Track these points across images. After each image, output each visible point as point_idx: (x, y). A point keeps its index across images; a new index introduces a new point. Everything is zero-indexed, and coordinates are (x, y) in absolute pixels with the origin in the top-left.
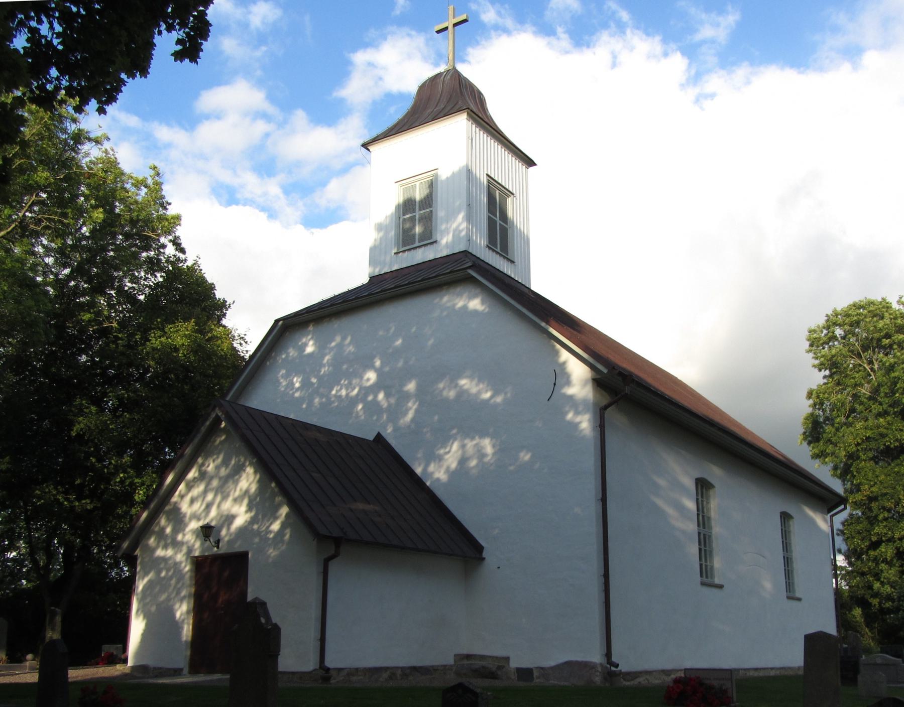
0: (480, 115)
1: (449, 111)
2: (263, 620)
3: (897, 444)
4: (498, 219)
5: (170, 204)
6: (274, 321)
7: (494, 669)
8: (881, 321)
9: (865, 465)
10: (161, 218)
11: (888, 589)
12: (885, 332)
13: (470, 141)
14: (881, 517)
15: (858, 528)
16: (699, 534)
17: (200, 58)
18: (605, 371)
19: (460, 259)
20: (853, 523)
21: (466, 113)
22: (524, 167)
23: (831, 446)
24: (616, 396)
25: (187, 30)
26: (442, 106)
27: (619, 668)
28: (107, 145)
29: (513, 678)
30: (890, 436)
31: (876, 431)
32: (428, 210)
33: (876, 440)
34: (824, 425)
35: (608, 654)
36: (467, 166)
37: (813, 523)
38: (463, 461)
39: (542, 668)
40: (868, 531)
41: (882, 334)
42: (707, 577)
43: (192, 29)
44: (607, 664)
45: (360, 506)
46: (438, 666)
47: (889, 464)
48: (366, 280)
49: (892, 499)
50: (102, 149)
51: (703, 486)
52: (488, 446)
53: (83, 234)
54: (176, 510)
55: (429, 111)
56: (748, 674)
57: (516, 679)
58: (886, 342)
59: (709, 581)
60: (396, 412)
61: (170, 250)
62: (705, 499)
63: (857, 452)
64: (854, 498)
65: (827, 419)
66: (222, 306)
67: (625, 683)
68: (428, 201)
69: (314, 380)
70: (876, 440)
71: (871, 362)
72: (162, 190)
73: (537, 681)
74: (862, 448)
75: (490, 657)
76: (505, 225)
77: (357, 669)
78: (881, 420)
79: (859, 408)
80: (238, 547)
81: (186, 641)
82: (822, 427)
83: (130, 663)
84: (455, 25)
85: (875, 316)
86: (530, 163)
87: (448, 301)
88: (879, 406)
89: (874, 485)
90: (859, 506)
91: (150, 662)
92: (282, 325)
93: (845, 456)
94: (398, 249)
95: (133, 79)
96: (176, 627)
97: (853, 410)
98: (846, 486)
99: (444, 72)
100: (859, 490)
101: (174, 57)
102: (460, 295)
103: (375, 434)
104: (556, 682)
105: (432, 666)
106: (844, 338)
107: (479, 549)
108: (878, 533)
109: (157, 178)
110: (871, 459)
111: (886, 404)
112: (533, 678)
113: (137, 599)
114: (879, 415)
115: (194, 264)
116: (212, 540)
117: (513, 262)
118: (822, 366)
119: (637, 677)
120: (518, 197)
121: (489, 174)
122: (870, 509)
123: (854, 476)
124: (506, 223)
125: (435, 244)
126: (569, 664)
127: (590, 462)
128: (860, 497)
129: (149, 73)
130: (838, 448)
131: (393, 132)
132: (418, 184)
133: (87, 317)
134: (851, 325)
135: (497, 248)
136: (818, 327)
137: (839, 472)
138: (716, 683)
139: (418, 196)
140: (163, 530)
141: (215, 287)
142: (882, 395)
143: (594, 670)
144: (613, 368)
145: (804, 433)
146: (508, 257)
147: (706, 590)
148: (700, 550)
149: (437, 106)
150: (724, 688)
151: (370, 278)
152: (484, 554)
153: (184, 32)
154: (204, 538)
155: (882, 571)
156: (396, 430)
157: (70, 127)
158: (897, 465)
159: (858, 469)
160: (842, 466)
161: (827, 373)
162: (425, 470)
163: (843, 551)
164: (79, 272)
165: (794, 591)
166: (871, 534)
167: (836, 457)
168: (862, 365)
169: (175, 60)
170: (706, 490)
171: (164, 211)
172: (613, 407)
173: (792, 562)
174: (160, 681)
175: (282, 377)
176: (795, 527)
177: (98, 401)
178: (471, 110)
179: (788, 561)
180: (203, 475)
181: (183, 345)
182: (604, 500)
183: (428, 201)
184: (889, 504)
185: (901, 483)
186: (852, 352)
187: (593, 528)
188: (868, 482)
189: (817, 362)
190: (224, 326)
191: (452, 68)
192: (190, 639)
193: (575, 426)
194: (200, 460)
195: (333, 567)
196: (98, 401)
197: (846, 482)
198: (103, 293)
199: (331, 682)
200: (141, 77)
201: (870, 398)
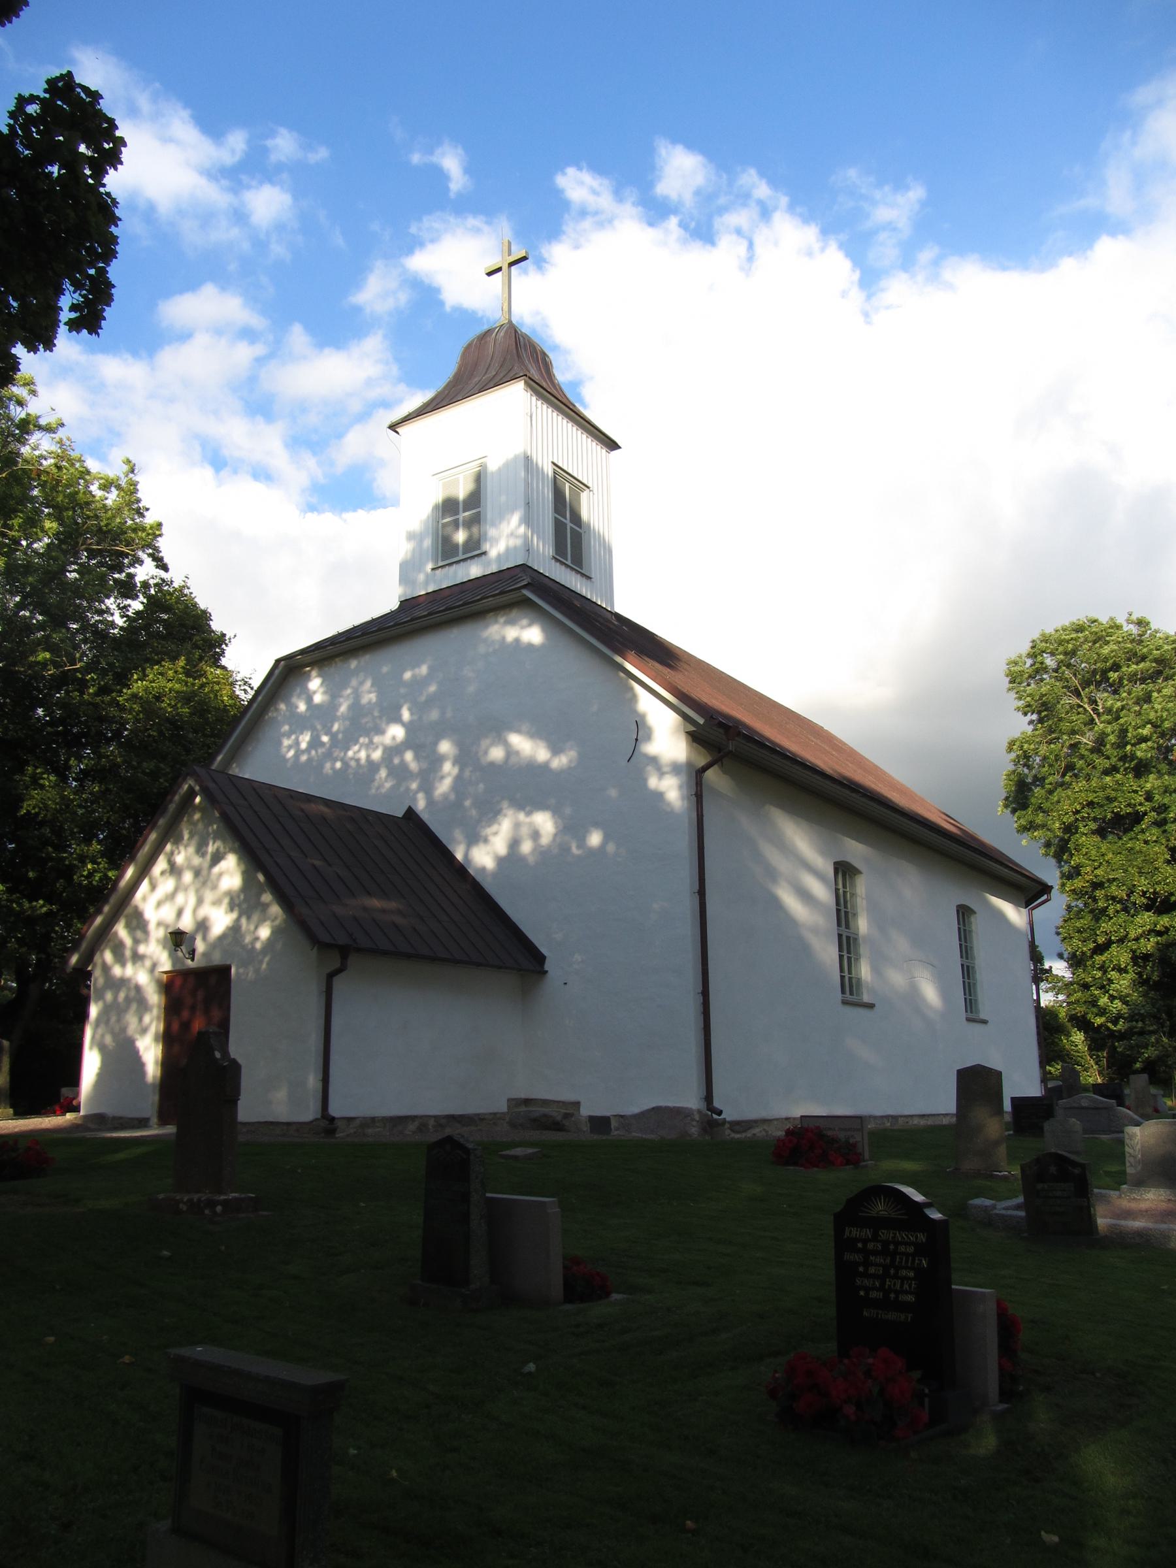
0: (544, 384)
1: (501, 379)
2: (218, 1055)
3: (1129, 810)
4: (568, 522)
5: (147, 509)
6: (274, 662)
7: (559, 1118)
8: (1106, 647)
9: (1086, 840)
10: (136, 529)
12: (1111, 661)
13: (529, 418)
14: (1111, 911)
15: (1078, 924)
16: (840, 936)
17: (102, 329)
18: (701, 721)
19: (515, 576)
20: (1072, 919)
22: (604, 451)
24: (719, 752)
25: (84, 292)
26: (494, 373)
28: (61, 434)
29: (585, 1129)
30: (1120, 799)
33: (1102, 806)
34: (1033, 788)
35: (709, 1098)
36: (525, 453)
37: (1000, 916)
38: (514, 844)
39: (622, 1116)
41: (1108, 664)
42: (851, 993)
43: (89, 292)
44: (708, 1110)
45: (376, 903)
46: (485, 1114)
47: (1120, 838)
48: (394, 605)
49: (1123, 885)
50: (55, 438)
51: (844, 871)
52: (545, 822)
55: (477, 379)
56: (910, 1123)
57: (589, 1130)
58: (1113, 676)
59: (854, 998)
62: (848, 889)
63: (1076, 822)
65: (1035, 778)
66: (221, 640)
67: (733, 1135)
69: (325, 739)
70: (1102, 806)
72: (138, 490)
73: (616, 1133)
75: (555, 1102)
76: (578, 529)
77: (373, 1119)
78: (1108, 779)
79: (1080, 763)
80: (217, 959)
81: (153, 1085)
84: (511, 264)
86: (612, 445)
88: (1105, 760)
89: (1099, 866)
90: (1080, 895)
92: (285, 666)
94: (437, 561)
95: (35, 353)
97: (1070, 767)
98: (1062, 869)
100: (1079, 874)
102: (512, 622)
103: (405, 809)
104: (640, 1135)
105: (478, 1115)
106: (1056, 671)
107: (540, 958)
108: (1106, 932)
109: (131, 475)
110: (1094, 832)
111: (1115, 757)
112: (611, 1129)
114: (1106, 772)
116: (184, 950)
117: (589, 578)
118: (1028, 709)
119: (750, 1128)
120: (595, 491)
121: (556, 462)
122: (1095, 900)
124: (580, 526)
125: (483, 556)
126: (657, 1110)
128: (1081, 884)
129: (55, 345)
130: (1050, 818)
131: (429, 409)
132: (461, 477)
135: (567, 560)
136: (1020, 657)
137: (1053, 849)
138: (842, 1136)
139: (462, 492)
141: (211, 616)
143: (689, 1118)
144: (712, 717)
145: (1007, 799)
146: (582, 572)
148: (841, 957)
149: (486, 372)
150: (851, 1141)
151: (401, 602)
152: (547, 967)
153: (80, 295)
154: (174, 947)
156: (430, 802)
157: (14, 411)
158: (1130, 839)
159: (1077, 845)
160: (1056, 842)
161: (1035, 717)
162: (466, 855)
165: (977, 1011)
167: (1048, 830)
168: (1082, 706)
170: (850, 877)
171: (141, 519)
172: (716, 767)
174: (115, 1135)
176: (978, 924)
177: (62, 773)
178: (529, 378)
179: (968, 972)
182: (702, 893)
183: (475, 499)
185: (1135, 863)
187: (687, 930)
189: (1021, 703)
190: (224, 668)
191: (507, 321)
193: (659, 796)
194: (168, 847)
195: (339, 983)
196: (62, 773)
197: (1063, 863)
199: (337, 1136)
200: (45, 351)
201: (1092, 751)
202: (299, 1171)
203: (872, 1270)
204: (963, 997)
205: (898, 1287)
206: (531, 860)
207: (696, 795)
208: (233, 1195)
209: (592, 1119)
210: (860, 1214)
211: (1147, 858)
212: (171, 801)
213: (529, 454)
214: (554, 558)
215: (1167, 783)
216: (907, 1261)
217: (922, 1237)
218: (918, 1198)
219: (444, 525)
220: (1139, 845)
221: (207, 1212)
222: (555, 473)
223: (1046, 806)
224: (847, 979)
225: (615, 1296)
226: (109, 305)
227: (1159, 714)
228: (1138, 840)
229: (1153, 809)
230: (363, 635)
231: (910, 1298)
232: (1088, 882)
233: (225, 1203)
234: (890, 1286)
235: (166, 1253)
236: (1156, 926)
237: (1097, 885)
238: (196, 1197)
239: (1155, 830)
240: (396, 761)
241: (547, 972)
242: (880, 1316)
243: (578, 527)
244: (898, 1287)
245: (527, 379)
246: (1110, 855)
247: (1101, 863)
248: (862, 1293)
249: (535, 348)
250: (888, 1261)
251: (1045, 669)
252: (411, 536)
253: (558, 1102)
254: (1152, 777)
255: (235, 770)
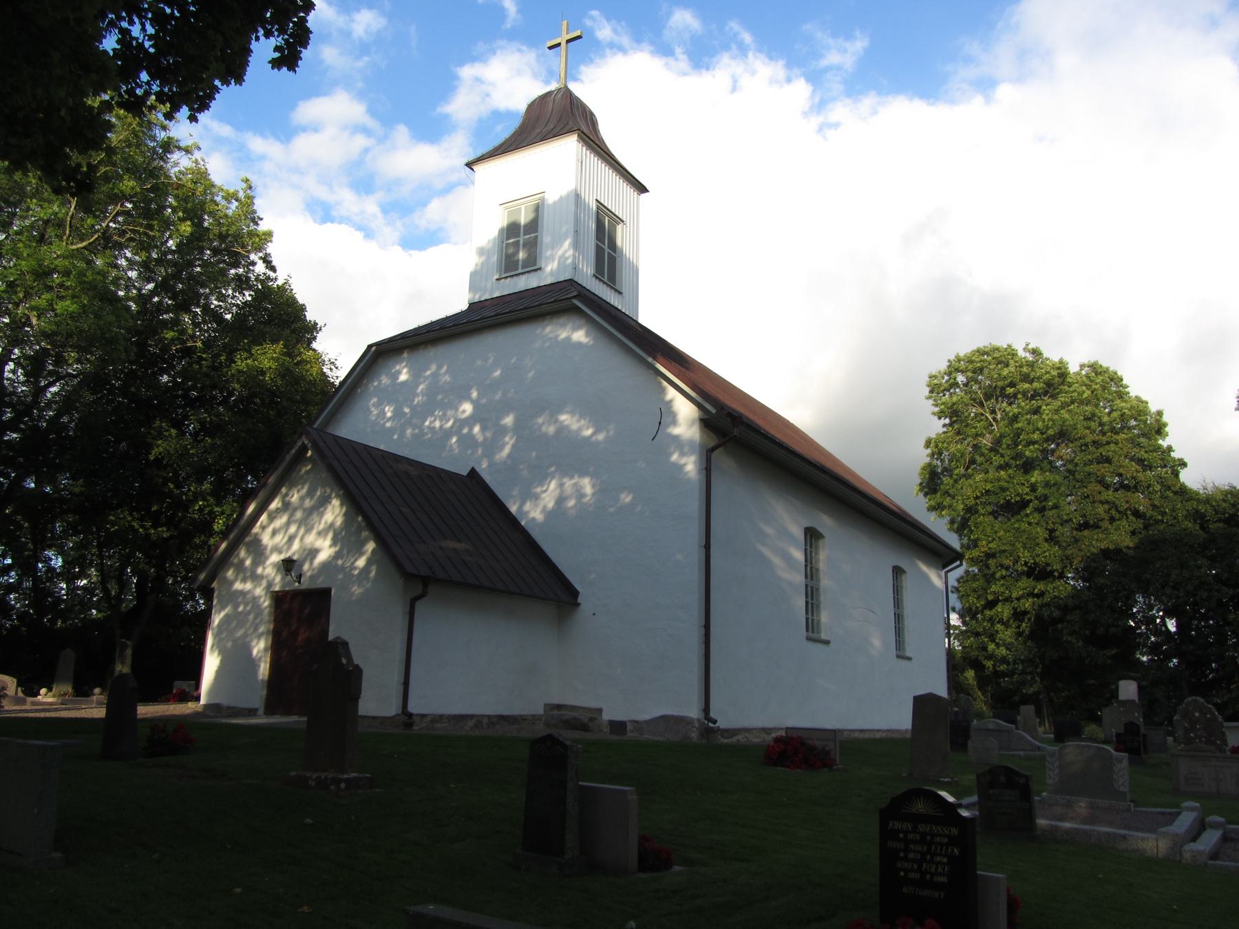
0: (591, 137)
2: (344, 661)
3: (1018, 499)
4: (606, 247)
5: (261, 219)
7: (586, 721)
10: (252, 234)
11: (1003, 651)
13: (580, 164)
14: (998, 575)
15: (974, 585)
16: (807, 586)
18: (714, 411)
21: (577, 135)
23: (948, 498)
24: (724, 437)
25: (286, 37)
26: (552, 126)
27: (717, 725)
28: (197, 155)
29: (605, 730)
31: (996, 484)
32: (533, 235)
33: (996, 494)
34: (942, 476)
35: (706, 710)
36: (576, 190)
38: (560, 500)
39: (636, 722)
40: (985, 590)
42: (813, 632)
45: (451, 544)
46: (527, 715)
49: (1011, 556)
51: (812, 535)
53: (169, 248)
54: (257, 541)
58: (1010, 390)
59: (815, 636)
60: (492, 446)
61: (260, 268)
64: (971, 554)
65: (945, 469)
67: (722, 740)
68: (533, 226)
69: (407, 410)
70: (996, 494)
71: (993, 412)
74: (981, 502)
75: (581, 708)
76: (613, 254)
77: (441, 716)
78: (1002, 473)
79: (979, 459)
80: (321, 583)
82: (940, 478)
83: (203, 701)
84: (568, 41)
85: (1000, 363)
86: (642, 189)
87: (550, 332)
89: (993, 541)
91: (224, 701)
92: (375, 350)
93: (963, 509)
94: (500, 275)
95: (228, 86)
96: (253, 664)
97: (973, 462)
99: (555, 90)
100: (976, 546)
101: (271, 65)
102: (563, 326)
105: (521, 716)
106: (966, 385)
107: (574, 593)
109: (249, 191)
110: (990, 513)
112: (627, 732)
113: (213, 634)
114: (1000, 467)
115: (285, 283)
116: (293, 575)
117: (620, 293)
122: (987, 567)
123: (972, 531)
126: (664, 718)
127: (694, 506)
128: (977, 554)
129: (244, 81)
132: (523, 207)
133: (170, 335)
134: (974, 372)
137: (956, 526)
139: (523, 219)
140: (242, 561)
142: (1004, 446)
143: (690, 726)
144: (723, 408)
145: (921, 484)
147: (811, 645)
148: (807, 603)
150: (827, 748)
152: (580, 600)
153: (283, 39)
154: (285, 572)
155: (997, 632)
161: (947, 421)
163: (957, 610)
164: (163, 287)
165: (904, 650)
166: (987, 593)
167: (954, 510)
169: (273, 68)
173: (903, 619)
174: (234, 721)
175: (374, 405)
176: (908, 582)
177: (178, 424)
180: (286, 506)
181: (270, 368)
183: (533, 226)
184: (1007, 562)
185: (1021, 540)
186: (974, 400)
188: (986, 537)
189: (936, 409)
192: (266, 677)
194: (284, 490)
195: (420, 607)
196: (178, 424)
197: (963, 537)
198: (188, 311)
200: (236, 85)
201: (991, 450)
202: (396, 756)
203: (911, 856)
204: (894, 625)
205: (933, 870)
206: (573, 512)
207: (706, 469)
208: (353, 774)
210: (903, 811)
211: (1031, 536)
212: (288, 453)
213: (579, 192)
214: (594, 275)
215: (1048, 478)
216: (941, 849)
217: (955, 831)
218: (951, 799)
219: (508, 245)
220: (1024, 526)
221: (332, 787)
222: (598, 208)
223: (951, 492)
224: (810, 621)
225: (676, 868)
226: (306, 48)
227: (1046, 423)
228: (1023, 522)
229: (1036, 498)
230: (441, 329)
231: (943, 879)
232: (983, 552)
233: (347, 781)
234: (926, 869)
235: (308, 821)
236: (1034, 590)
237: (990, 555)
238: (323, 775)
239: (1036, 515)
240: (465, 431)
241: (579, 604)
242: (917, 893)
243: (612, 251)
244: (933, 870)
245: (580, 133)
246: (1002, 533)
247: (994, 539)
248: (902, 874)
249: (585, 108)
250: (925, 849)
251: (956, 385)
252: (481, 252)
253: (585, 708)
254: (1036, 473)
255: (331, 430)
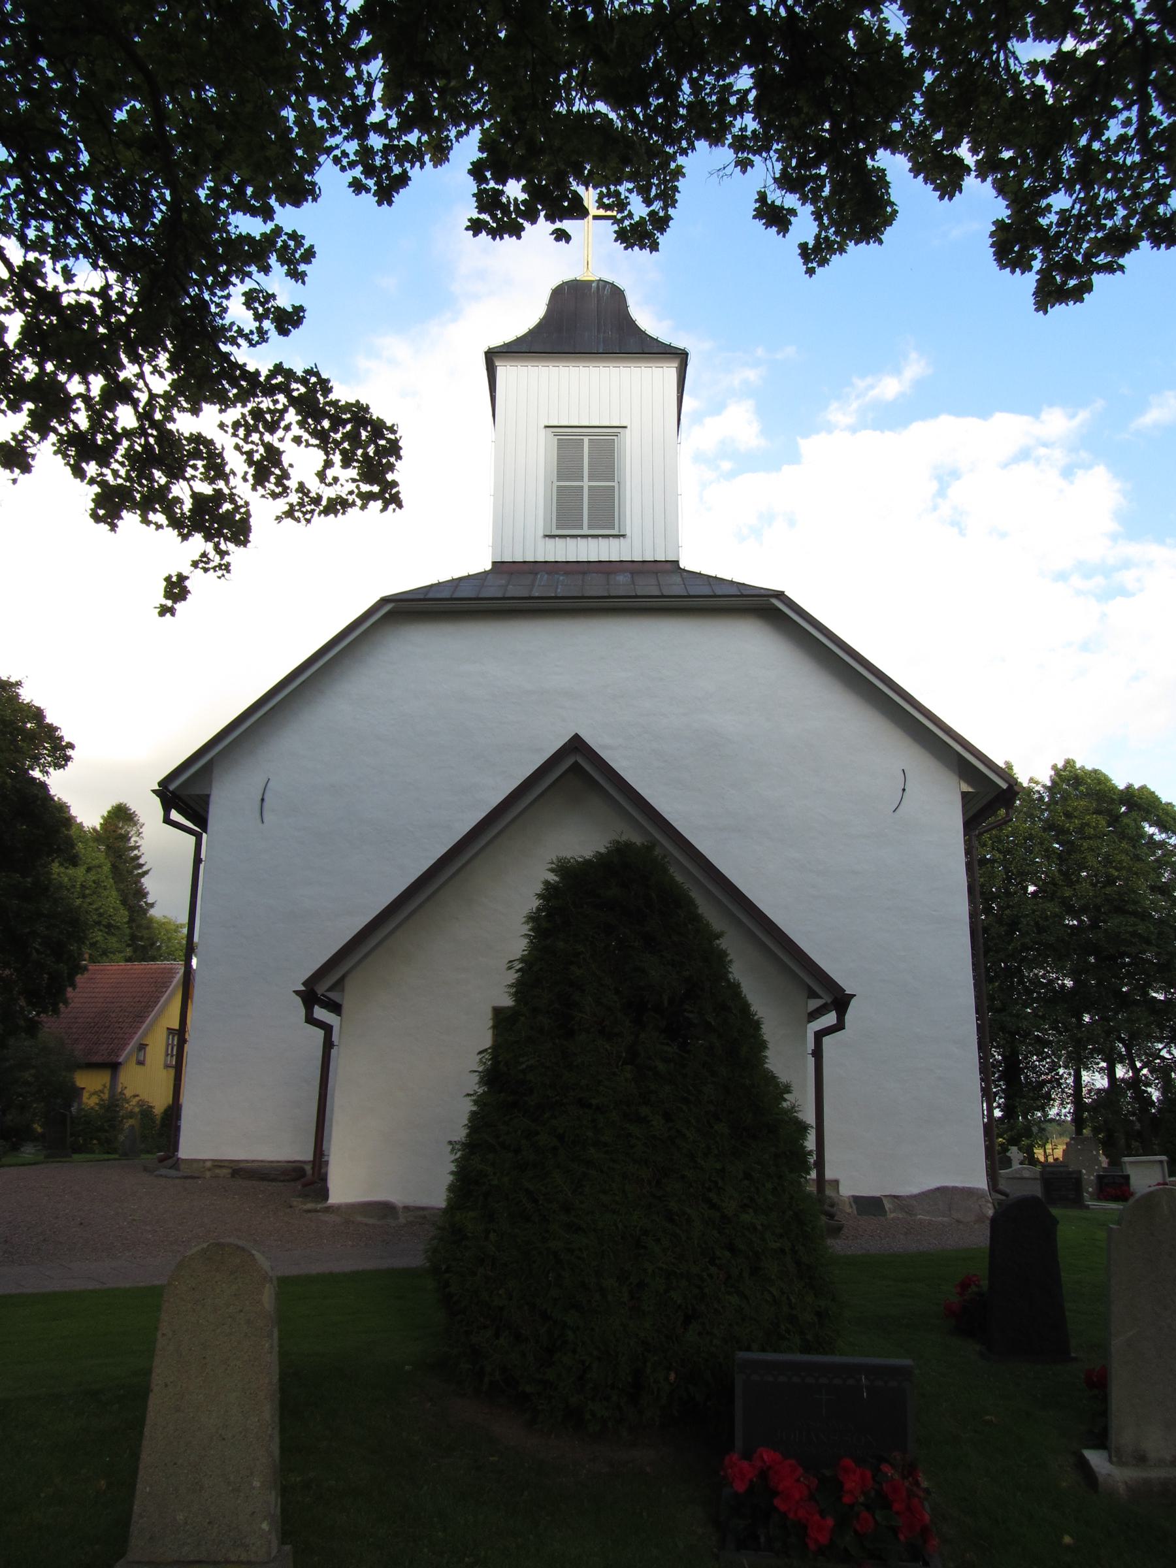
29: (849, 1210)
39: (895, 1197)
57: (855, 1212)
73: (892, 1215)
112: (886, 1212)
126: (941, 1190)
143: (983, 1200)
209: (857, 1200)
